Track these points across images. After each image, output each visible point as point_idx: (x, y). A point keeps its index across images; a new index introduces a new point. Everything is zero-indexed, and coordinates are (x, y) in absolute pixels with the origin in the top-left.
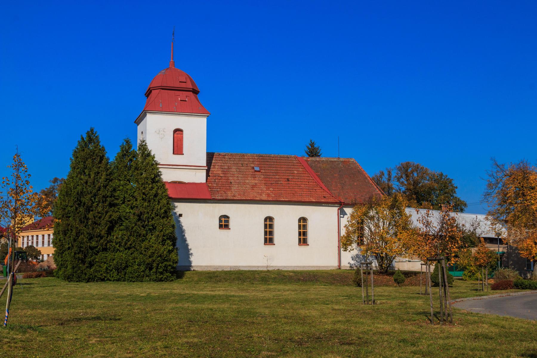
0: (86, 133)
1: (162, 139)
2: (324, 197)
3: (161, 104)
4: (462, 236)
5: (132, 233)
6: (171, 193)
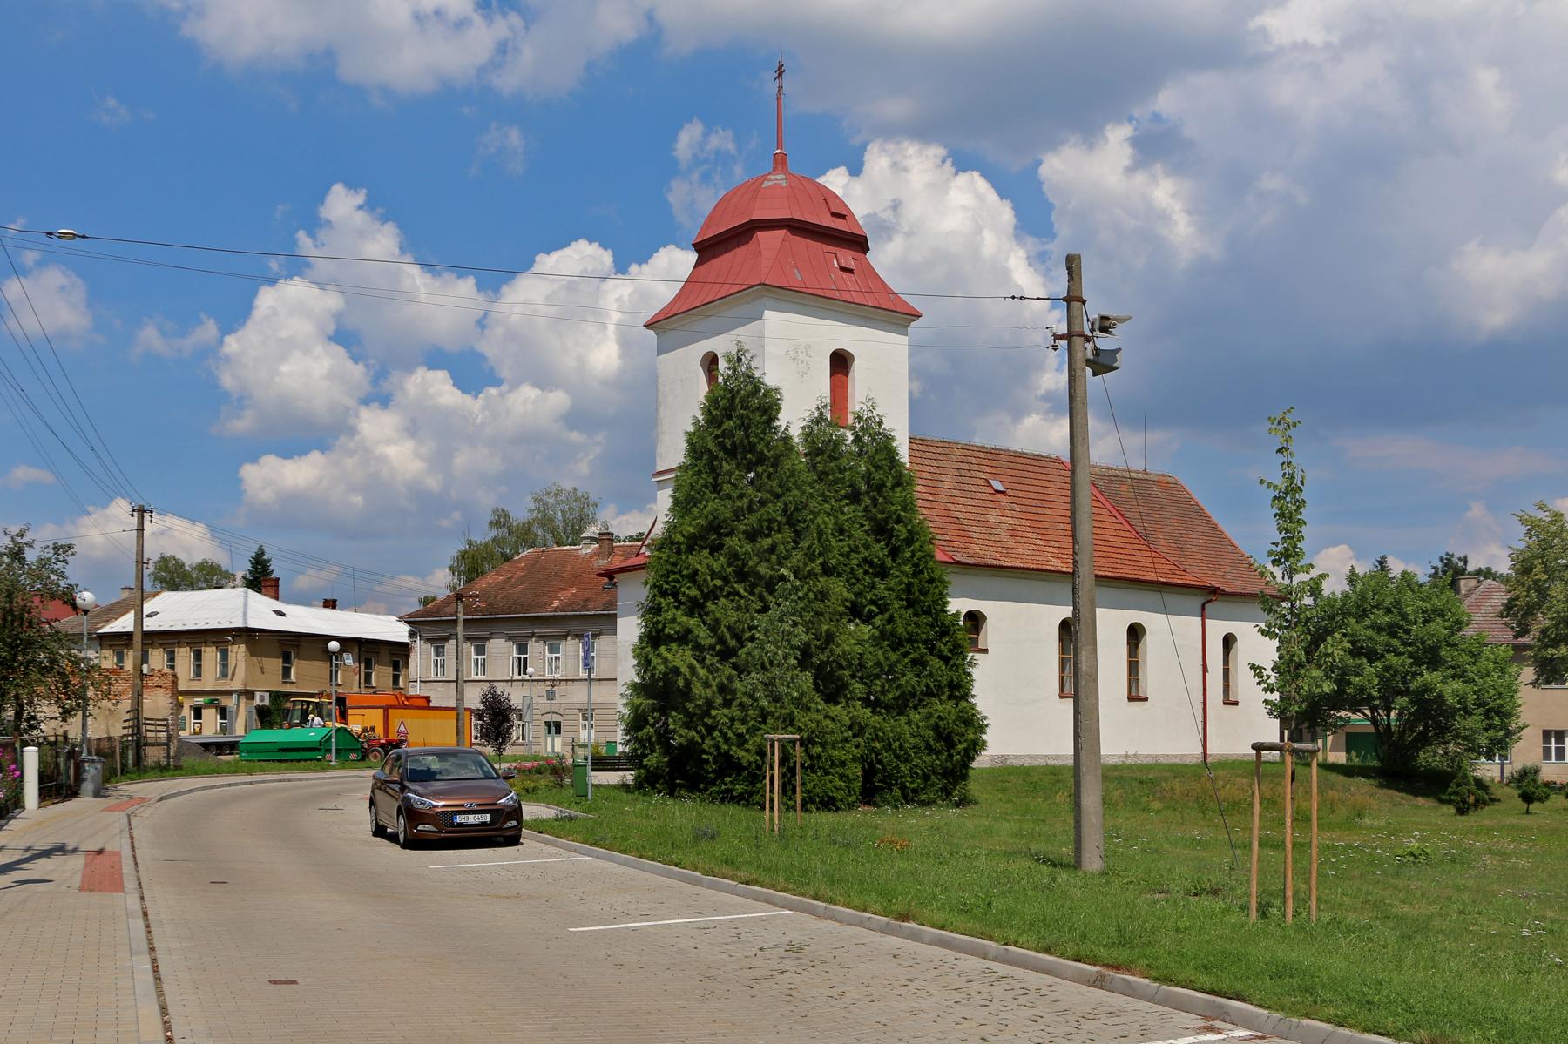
1: (802, 376)
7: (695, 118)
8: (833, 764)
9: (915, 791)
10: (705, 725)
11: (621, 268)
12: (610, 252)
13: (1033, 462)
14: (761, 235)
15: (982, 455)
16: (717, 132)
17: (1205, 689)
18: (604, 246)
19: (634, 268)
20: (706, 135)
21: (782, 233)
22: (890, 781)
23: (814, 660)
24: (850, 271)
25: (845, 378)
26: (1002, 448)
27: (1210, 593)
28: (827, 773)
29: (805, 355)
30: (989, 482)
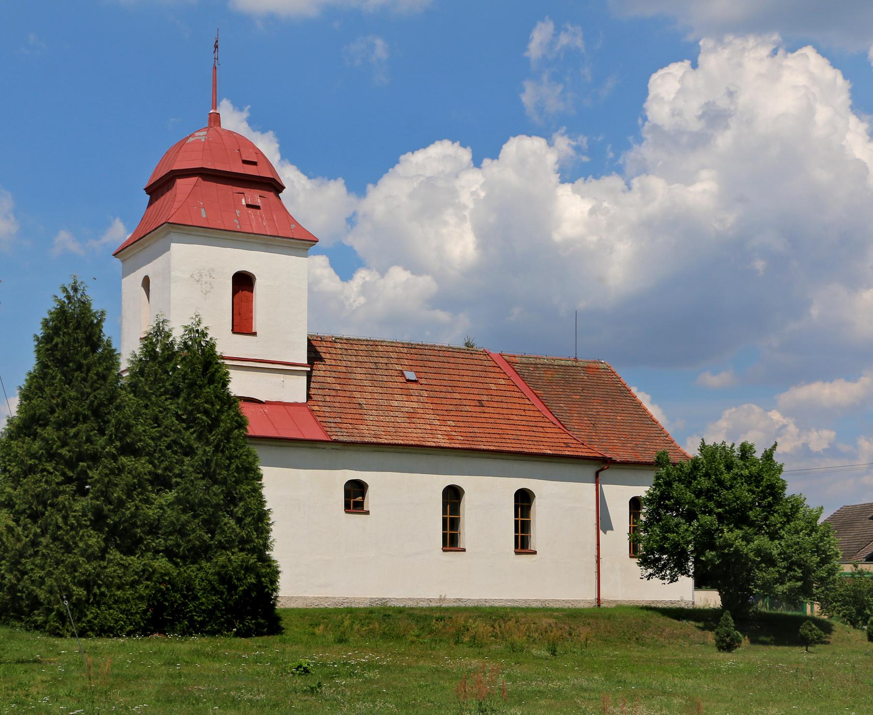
0: (280, 572)
1: (206, 294)
2: (567, 445)
3: (203, 210)
4: (112, 411)
5: (161, 325)
6: (254, 428)
7: (547, 17)
8: (116, 602)
9: (201, 623)
10: (18, 570)
11: (477, 162)
12: (469, 149)
13: (457, 355)
14: (180, 182)
15: (406, 350)
16: (566, 30)
17: (598, 544)
18: (463, 145)
19: (487, 162)
20: (556, 35)
21: (193, 180)
22: (178, 613)
23: (109, 521)
24: (258, 207)
25: (250, 293)
26: (428, 344)
27: (603, 463)
28: (110, 608)
29: (208, 277)
30: (403, 374)
